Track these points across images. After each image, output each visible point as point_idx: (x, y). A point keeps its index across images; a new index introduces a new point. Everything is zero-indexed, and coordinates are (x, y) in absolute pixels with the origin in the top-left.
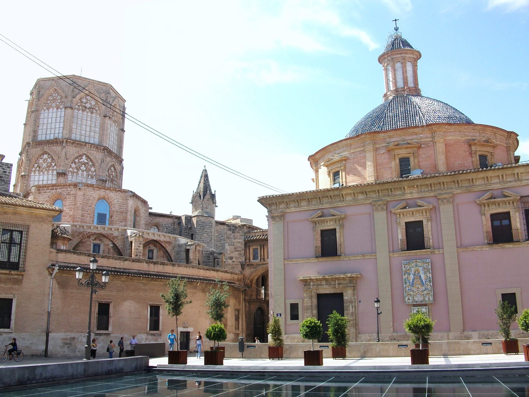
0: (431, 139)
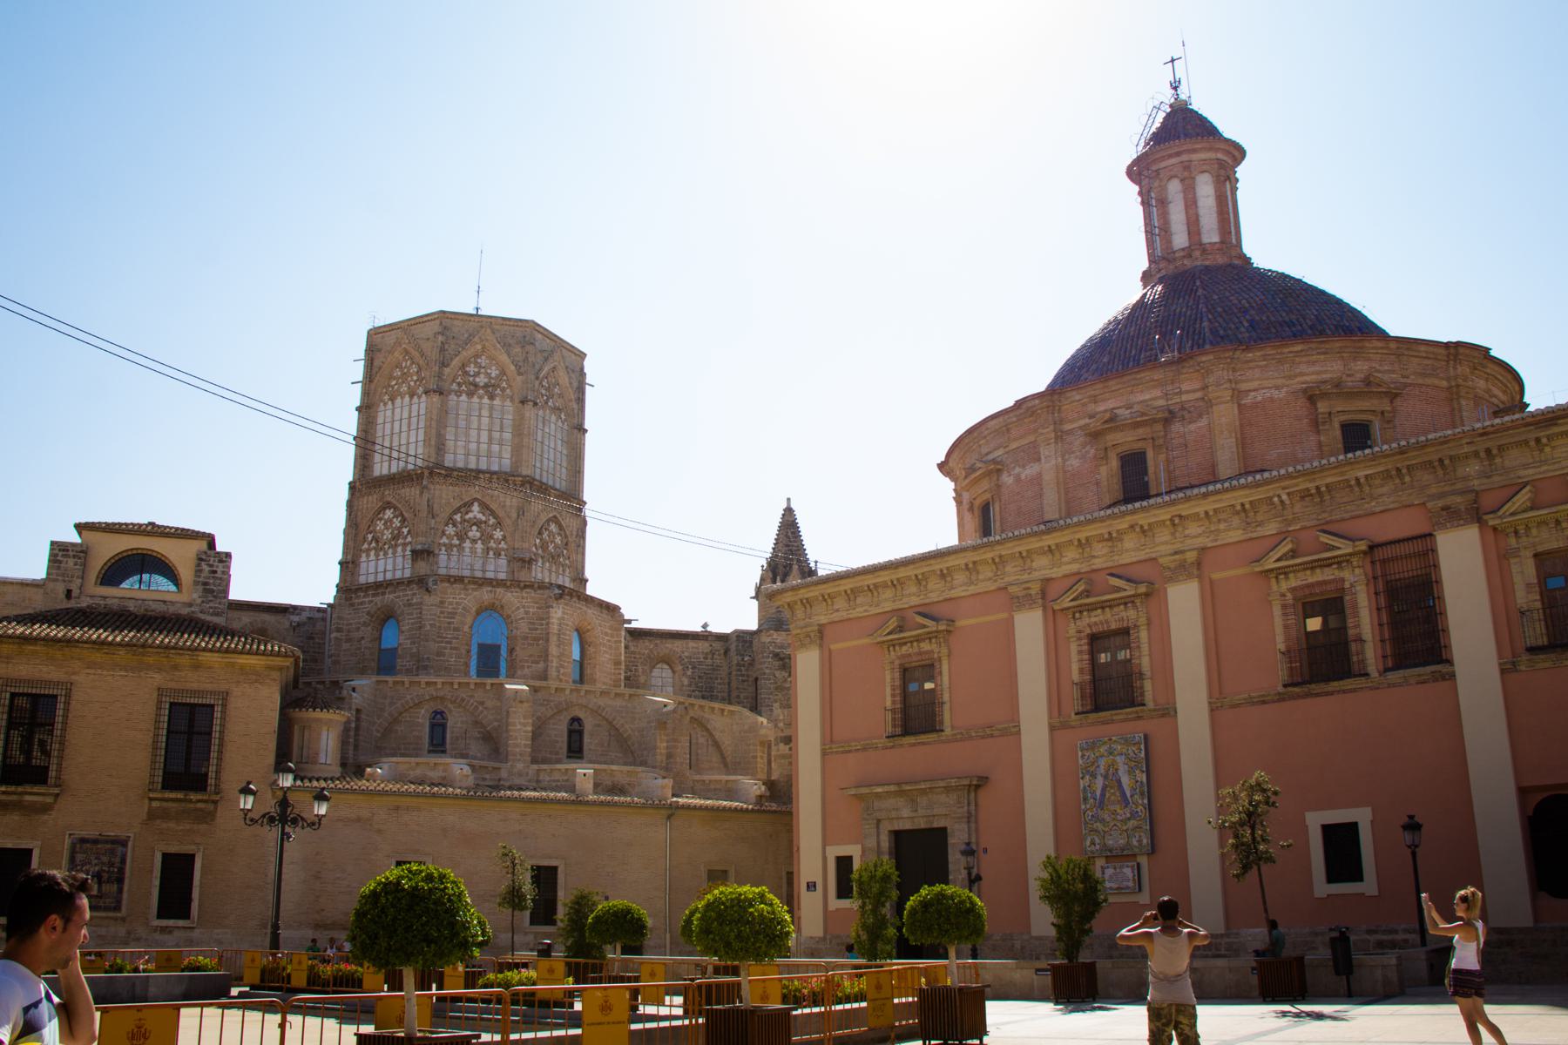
0: (1199, 395)
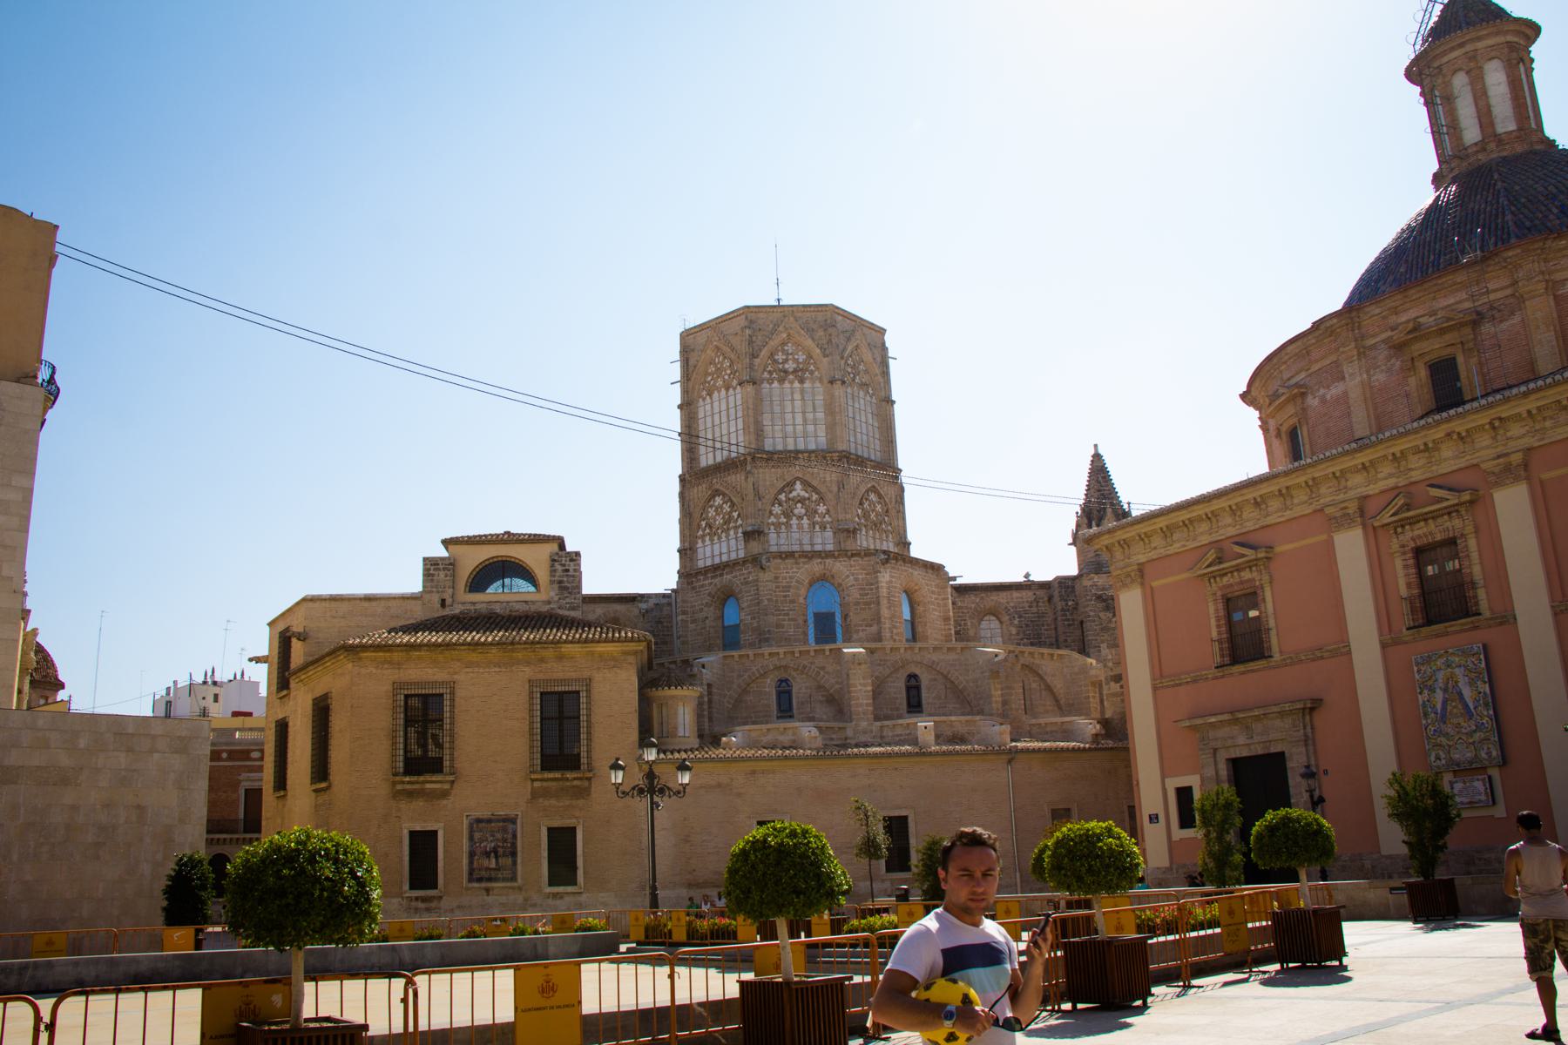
0: (1509, 292)
